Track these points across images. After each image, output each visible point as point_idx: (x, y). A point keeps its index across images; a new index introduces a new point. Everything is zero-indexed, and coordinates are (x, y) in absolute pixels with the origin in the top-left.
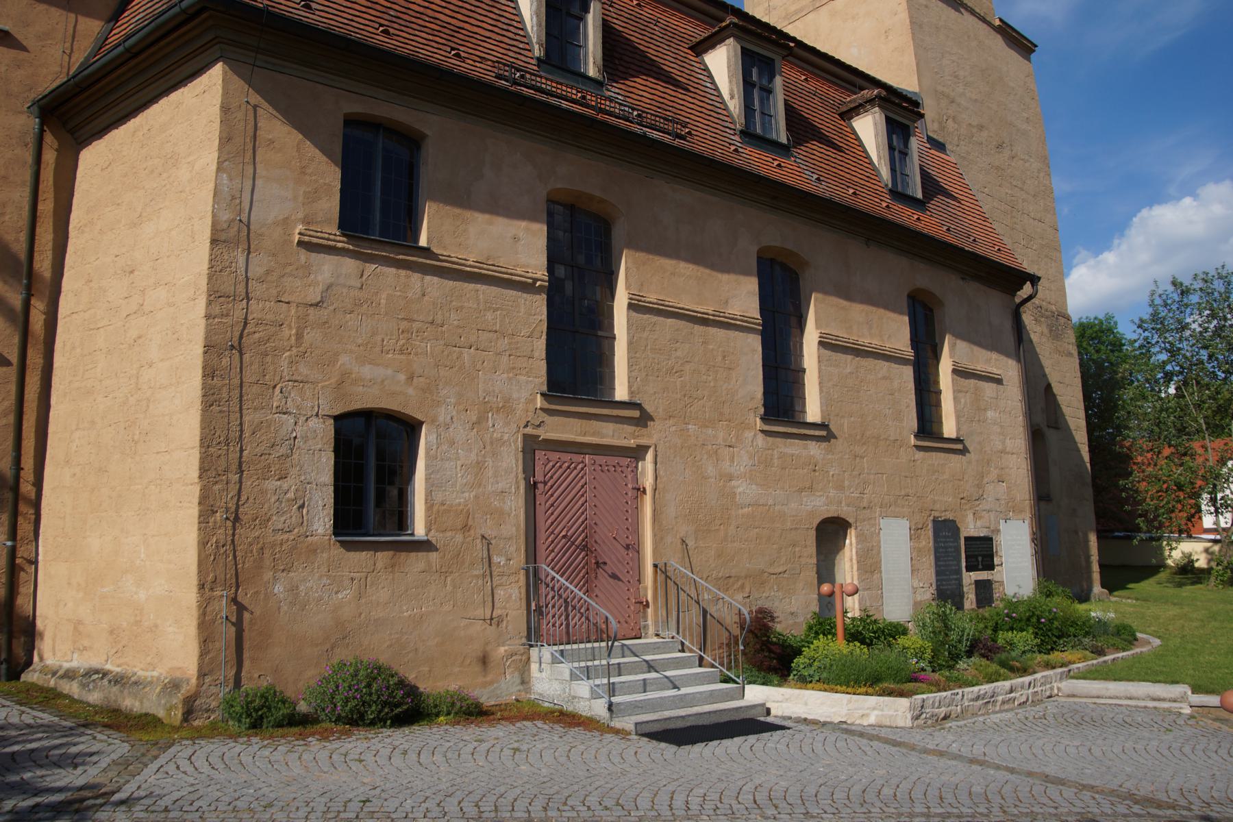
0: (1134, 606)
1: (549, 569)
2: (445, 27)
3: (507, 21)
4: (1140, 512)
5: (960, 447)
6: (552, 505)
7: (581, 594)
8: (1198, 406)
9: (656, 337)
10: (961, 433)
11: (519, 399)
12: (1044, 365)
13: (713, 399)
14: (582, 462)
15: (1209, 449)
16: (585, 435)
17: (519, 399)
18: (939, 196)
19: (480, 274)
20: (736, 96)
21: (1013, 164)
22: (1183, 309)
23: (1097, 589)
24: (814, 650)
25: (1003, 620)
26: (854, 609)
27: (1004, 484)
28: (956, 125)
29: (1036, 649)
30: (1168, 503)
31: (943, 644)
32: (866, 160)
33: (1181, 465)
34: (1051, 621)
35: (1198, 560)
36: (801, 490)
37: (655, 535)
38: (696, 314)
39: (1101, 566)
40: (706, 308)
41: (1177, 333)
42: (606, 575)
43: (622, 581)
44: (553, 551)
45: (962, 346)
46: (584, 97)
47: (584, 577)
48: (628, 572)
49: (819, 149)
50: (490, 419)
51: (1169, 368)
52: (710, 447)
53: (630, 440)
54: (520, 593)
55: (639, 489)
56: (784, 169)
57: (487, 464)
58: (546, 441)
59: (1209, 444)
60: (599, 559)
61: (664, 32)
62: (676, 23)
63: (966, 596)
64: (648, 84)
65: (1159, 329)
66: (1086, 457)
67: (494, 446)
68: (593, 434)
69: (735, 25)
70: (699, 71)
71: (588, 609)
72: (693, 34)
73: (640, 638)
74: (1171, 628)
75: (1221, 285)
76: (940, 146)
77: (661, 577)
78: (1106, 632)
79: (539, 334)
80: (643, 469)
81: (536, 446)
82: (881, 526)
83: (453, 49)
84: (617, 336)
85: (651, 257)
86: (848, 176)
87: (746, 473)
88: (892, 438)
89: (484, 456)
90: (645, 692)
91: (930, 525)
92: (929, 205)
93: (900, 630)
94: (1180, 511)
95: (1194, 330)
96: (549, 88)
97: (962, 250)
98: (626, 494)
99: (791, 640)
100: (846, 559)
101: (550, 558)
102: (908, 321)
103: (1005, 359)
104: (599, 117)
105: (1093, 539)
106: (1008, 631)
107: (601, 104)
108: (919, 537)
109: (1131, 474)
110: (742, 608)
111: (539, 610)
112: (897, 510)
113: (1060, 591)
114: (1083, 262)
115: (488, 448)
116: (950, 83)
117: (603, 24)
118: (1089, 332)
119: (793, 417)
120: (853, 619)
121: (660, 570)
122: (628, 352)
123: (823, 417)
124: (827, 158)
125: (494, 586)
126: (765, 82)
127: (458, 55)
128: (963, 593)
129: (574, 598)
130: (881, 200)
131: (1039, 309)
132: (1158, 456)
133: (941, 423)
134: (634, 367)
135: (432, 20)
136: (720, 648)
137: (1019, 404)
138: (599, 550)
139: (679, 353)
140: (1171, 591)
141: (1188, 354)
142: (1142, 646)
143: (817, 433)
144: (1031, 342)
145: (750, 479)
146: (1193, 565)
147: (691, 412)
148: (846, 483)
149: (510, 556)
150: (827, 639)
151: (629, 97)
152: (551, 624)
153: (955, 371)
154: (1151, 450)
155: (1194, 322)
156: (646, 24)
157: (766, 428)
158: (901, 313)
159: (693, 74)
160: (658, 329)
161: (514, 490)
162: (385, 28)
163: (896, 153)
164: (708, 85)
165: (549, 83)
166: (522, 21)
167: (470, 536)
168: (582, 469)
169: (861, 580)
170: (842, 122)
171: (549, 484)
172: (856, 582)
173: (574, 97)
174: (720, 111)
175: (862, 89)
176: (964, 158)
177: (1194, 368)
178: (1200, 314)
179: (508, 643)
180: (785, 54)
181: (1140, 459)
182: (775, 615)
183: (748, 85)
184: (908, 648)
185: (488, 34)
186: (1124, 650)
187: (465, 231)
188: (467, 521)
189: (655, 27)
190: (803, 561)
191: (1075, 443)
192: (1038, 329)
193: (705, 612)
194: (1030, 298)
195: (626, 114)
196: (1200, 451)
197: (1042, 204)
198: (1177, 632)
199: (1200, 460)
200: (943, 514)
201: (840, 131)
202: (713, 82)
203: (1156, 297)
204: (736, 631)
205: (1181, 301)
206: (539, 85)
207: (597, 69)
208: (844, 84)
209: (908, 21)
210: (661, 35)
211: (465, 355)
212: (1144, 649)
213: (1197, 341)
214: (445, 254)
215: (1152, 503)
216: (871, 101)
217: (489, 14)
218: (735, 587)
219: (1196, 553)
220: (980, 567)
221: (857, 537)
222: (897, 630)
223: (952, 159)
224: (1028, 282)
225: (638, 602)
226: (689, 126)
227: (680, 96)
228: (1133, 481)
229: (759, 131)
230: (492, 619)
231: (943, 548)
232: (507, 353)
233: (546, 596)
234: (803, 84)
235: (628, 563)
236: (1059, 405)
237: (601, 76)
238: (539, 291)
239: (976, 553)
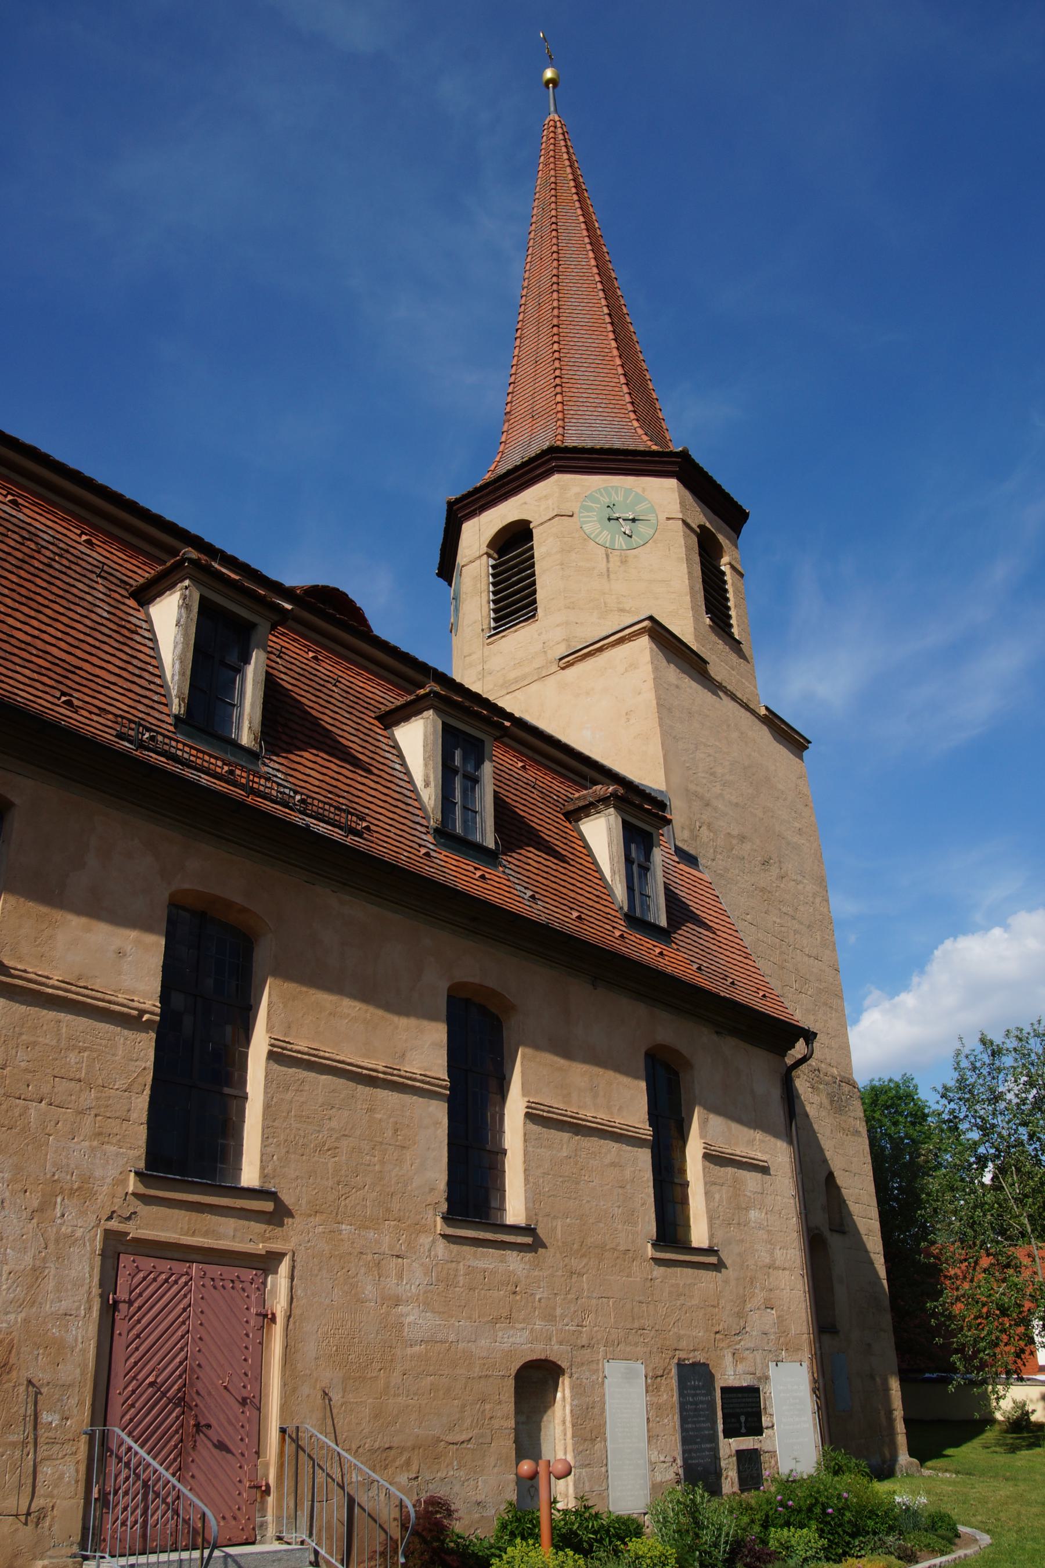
0: (954, 1483)
1: (124, 1435)
2: (57, 665)
3: (140, 664)
4: (955, 1345)
5: (713, 1260)
6: (138, 1336)
7: (167, 1475)
8: (1020, 1201)
9: (302, 1099)
10: (715, 1241)
11: (103, 1178)
12: (824, 1147)
13: (378, 1190)
14: (187, 1273)
15: (1037, 1259)
16: (193, 1234)
17: (103, 1178)
18: (688, 924)
19: (66, 998)
20: (432, 784)
21: (782, 886)
22: (995, 1074)
23: (904, 1458)
24: (508, 1562)
25: (776, 1511)
26: (567, 1496)
27: (774, 1312)
28: (712, 834)
29: (822, 1554)
30: (990, 1333)
31: (692, 1549)
32: (596, 874)
33: (1004, 1280)
34: (841, 1511)
35: (1034, 1411)
36: (496, 1321)
37: (284, 1385)
38: (360, 1070)
39: (906, 1421)
40: (376, 1063)
41: (989, 1104)
43: (233, 1454)
44: (133, 1405)
45: (716, 1122)
46: (231, 772)
47: (176, 1446)
48: (242, 1440)
49: (536, 858)
50: (58, 1206)
51: (982, 1150)
52: (370, 1257)
53: (257, 1244)
54: (77, 1471)
56: (489, 882)
57: (47, 1271)
58: (137, 1241)
59: (1036, 1252)
60: (200, 1419)
61: (345, 695)
62: (361, 685)
63: (724, 1474)
64: (319, 760)
65: (968, 1100)
66: (882, 1272)
67: (61, 1245)
68: (206, 1234)
69: (436, 694)
70: (387, 748)
71: (178, 1498)
72: (382, 700)
73: (253, 1543)
74: (1003, 1516)
75: (1038, 1045)
76: (691, 860)
77: (289, 1448)
78: (916, 1526)
79: (141, 1088)
80: (274, 1285)
81: (121, 1248)
82: (606, 1373)
83: (64, 694)
84: (249, 1096)
85: (304, 989)
86: (572, 895)
87: (419, 1295)
88: (622, 1248)
91: (674, 1371)
92: (675, 935)
93: (632, 1528)
94: (1006, 1345)
95: (1010, 1101)
96: (186, 756)
97: (717, 996)
98: (247, 1322)
99: (475, 1545)
100: (556, 1421)
101: (128, 1417)
102: (645, 1088)
103: (773, 1139)
104: (249, 800)
105: (895, 1385)
106: (782, 1527)
107: (253, 782)
108: (658, 1389)
109: (941, 1293)
110: (404, 1498)
111: (104, 1500)
112: (628, 1349)
113: (852, 1465)
114: (876, 1005)
115: (52, 1246)
116: (704, 781)
117: (266, 679)
118: (883, 1098)
119: (487, 1217)
120: (565, 1512)
121: (290, 1436)
122: (264, 1119)
123: (528, 1217)
124: (546, 869)
125: (38, 1460)
126: (470, 768)
127: (69, 703)
128: (721, 1470)
129: (159, 1479)
130: (614, 927)
131: (817, 1072)
132: (974, 1269)
133: (689, 1226)
134: (270, 1140)
135: (41, 654)
136: (371, 1559)
137: (792, 1201)
138: (201, 1405)
139: (334, 1124)
140: (1002, 1459)
141: (1005, 1133)
142: (967, 1545)
143: (520, 1239)
144: (807, 1116)
145: (424, 1304)
146: (1029, 1418)
147: (346, 1206)
148: (559, 1311)
150: (528, 1545)
151: (292, 776)
152: (119, 1522)
153: (707, 1156)
154: (965, 1260)
155: (1009, 1091)
156: (322, 683)
157: (450, 1231)
158: (636, 1077)
159: (378, 751)
160: (307, 1088)
161: (83, 1312)
162: (88, 537)
163: (635, 867)
164: (398, 767)
165: (187, 749)
166: (160, 666)
167: (9, 1381)
168: (186, 1284)
169: (577, 1453)
170: (567, 824)
171: (136, 1305)
172: (570, 1458)
173: (219, 770)
174: (410, 801)
175: (595, 783)
176: (722, 876)
177: (1013, 1150)
178: (1016, 1081)
179: (48, 1553)
180: (498, 734)
181: (952, 1272)
182: (453, 1507)
183: (448, 771)
184: (642, 1557)
185: (113, 679)
186: (943, 1553)
187: (51, 937)
188: (8, 1357)
189: (334, 688)
190: (496, 1423)
191: (867, 1251)
192: (816, 1099)
193: (351, 1501)
194: (804, 1060)
195: (286, 797)
196: (1026, 1261)
197: (818, 937)
198: (1011, 1523)
199: (1026, 1274)
200: (691, 1355)
201: (564, 835)
202: (404, 764)
203: (962, 1057)
204: (396, 1532)
205: (993, 1065)
206: (173, 750)
207: (252, 736)
208: (571, 775)
209: (655, 702)
210: (341, 699)
211: (32, 1111)
212: (969, 1552)
213: (1014, 1116)
214: (19, 967)
215: (969, 1334)
216: (605, 800)
217: (118, 653)
218: (397, 1463)
219: (1031, 1401)
220: (743, 1430)
221: (572, 1388)
222: (631, 1529)
223: (706, 877)
224: (801, 1040)
226: (368, 818)
227: (359, 779)
228: (945, 1303)
229: (459, 830)
230: (28, 1514)
231: (691, 1403)
232: (93, 1112)
233: (116, 1477)
234: (520, 772)
235: (242, 1426)
236: (844, 1201)
237: (257, 746)
238: (146, 1027)
239: (738, 1410)
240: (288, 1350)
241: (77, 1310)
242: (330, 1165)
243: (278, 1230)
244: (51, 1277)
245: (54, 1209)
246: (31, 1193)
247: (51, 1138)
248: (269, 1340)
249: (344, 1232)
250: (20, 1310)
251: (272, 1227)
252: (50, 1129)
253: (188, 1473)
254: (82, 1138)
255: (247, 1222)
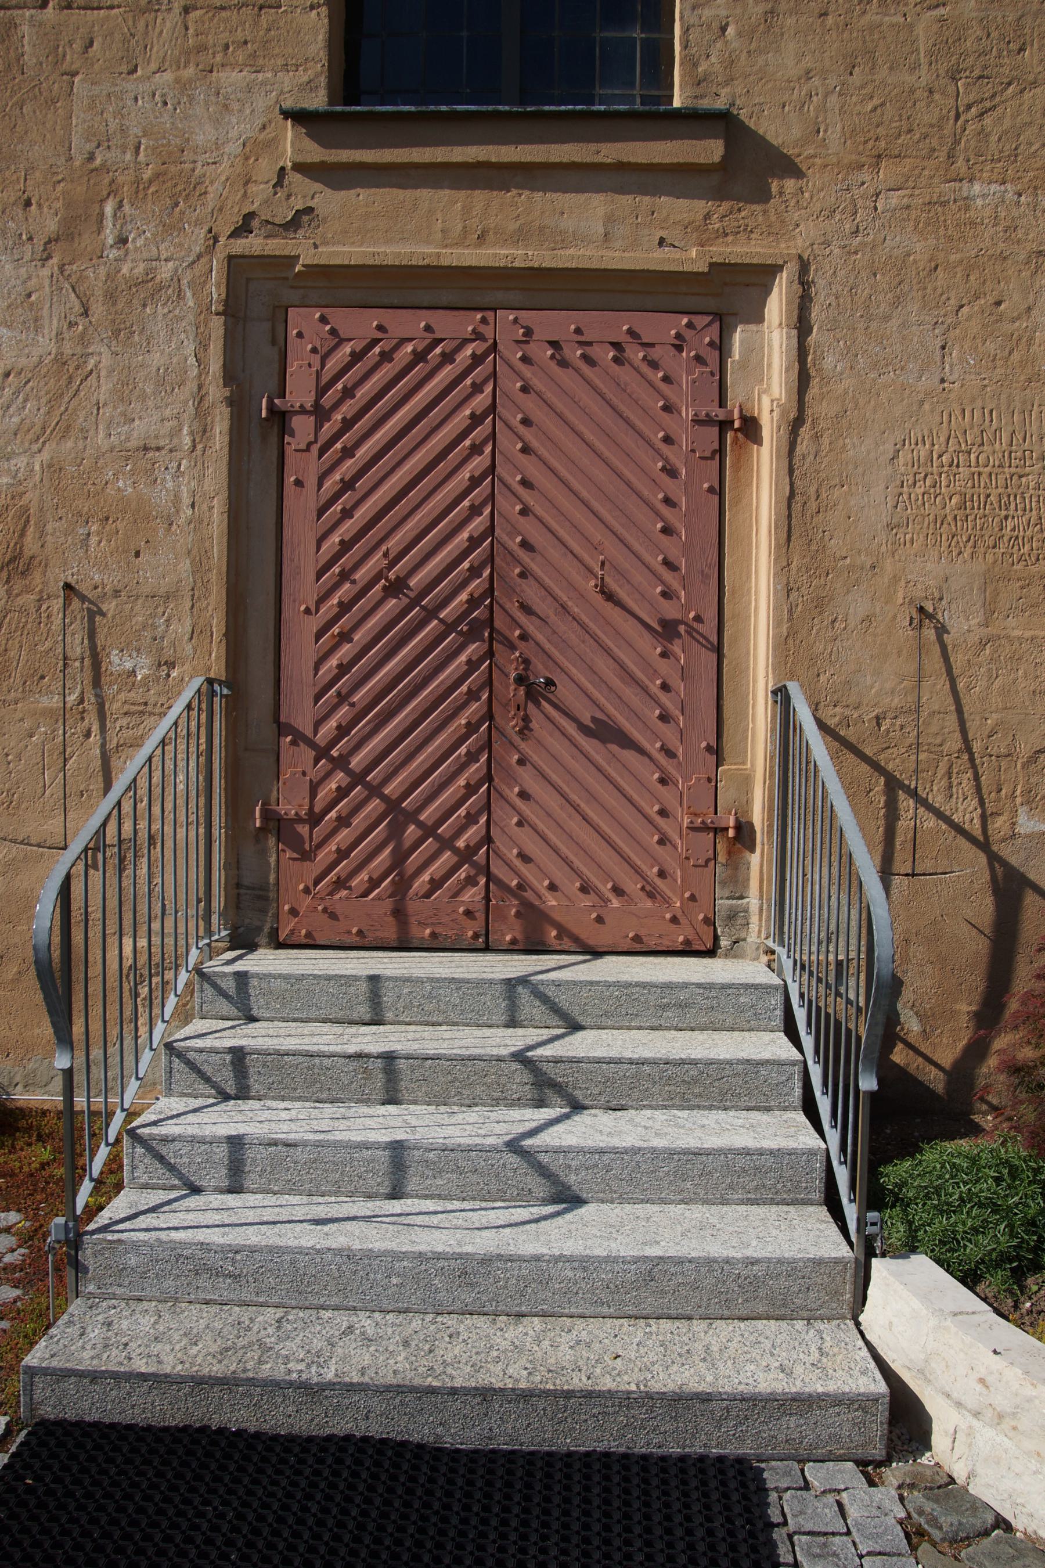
6: (348, 485)
14: (478, 336)
42: (571, 729)
50: (108, 222)
55: (724, 425)
57: (92, 362)
67: (120, 306)
68: (520, 237)
73: (711, 953)
89: (83, 339)
90: (396, 1194)
101: (333, 662)
115: (98, 310)
149: (168, 654)
161: (187, 441)
168: (477, 360)
225: (705, 828)
240: (797, 507)
241: (171, 436)
242: (920, 30)
243: (751, 213)
244: (103, 373)
245: (100, 229)
246: (40, 206)
247: (77, 80)
248: (744, 484)
249: (979, 202)
250: (35, 447)
251: (726, 205)
252: (72, 59)
253: (511, 788)
254: (153, 66)
255: (647, 199)
